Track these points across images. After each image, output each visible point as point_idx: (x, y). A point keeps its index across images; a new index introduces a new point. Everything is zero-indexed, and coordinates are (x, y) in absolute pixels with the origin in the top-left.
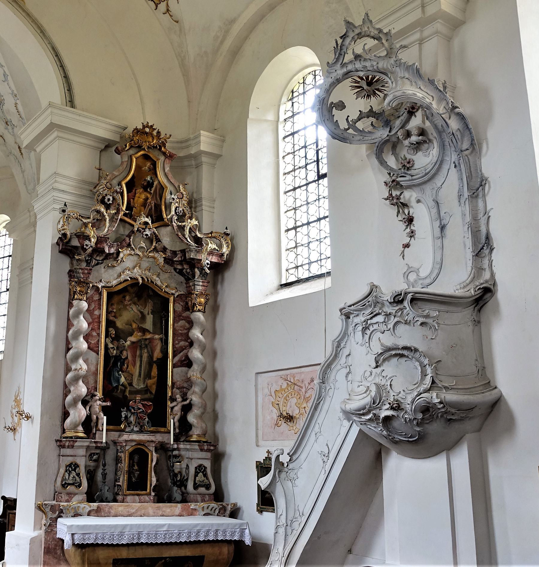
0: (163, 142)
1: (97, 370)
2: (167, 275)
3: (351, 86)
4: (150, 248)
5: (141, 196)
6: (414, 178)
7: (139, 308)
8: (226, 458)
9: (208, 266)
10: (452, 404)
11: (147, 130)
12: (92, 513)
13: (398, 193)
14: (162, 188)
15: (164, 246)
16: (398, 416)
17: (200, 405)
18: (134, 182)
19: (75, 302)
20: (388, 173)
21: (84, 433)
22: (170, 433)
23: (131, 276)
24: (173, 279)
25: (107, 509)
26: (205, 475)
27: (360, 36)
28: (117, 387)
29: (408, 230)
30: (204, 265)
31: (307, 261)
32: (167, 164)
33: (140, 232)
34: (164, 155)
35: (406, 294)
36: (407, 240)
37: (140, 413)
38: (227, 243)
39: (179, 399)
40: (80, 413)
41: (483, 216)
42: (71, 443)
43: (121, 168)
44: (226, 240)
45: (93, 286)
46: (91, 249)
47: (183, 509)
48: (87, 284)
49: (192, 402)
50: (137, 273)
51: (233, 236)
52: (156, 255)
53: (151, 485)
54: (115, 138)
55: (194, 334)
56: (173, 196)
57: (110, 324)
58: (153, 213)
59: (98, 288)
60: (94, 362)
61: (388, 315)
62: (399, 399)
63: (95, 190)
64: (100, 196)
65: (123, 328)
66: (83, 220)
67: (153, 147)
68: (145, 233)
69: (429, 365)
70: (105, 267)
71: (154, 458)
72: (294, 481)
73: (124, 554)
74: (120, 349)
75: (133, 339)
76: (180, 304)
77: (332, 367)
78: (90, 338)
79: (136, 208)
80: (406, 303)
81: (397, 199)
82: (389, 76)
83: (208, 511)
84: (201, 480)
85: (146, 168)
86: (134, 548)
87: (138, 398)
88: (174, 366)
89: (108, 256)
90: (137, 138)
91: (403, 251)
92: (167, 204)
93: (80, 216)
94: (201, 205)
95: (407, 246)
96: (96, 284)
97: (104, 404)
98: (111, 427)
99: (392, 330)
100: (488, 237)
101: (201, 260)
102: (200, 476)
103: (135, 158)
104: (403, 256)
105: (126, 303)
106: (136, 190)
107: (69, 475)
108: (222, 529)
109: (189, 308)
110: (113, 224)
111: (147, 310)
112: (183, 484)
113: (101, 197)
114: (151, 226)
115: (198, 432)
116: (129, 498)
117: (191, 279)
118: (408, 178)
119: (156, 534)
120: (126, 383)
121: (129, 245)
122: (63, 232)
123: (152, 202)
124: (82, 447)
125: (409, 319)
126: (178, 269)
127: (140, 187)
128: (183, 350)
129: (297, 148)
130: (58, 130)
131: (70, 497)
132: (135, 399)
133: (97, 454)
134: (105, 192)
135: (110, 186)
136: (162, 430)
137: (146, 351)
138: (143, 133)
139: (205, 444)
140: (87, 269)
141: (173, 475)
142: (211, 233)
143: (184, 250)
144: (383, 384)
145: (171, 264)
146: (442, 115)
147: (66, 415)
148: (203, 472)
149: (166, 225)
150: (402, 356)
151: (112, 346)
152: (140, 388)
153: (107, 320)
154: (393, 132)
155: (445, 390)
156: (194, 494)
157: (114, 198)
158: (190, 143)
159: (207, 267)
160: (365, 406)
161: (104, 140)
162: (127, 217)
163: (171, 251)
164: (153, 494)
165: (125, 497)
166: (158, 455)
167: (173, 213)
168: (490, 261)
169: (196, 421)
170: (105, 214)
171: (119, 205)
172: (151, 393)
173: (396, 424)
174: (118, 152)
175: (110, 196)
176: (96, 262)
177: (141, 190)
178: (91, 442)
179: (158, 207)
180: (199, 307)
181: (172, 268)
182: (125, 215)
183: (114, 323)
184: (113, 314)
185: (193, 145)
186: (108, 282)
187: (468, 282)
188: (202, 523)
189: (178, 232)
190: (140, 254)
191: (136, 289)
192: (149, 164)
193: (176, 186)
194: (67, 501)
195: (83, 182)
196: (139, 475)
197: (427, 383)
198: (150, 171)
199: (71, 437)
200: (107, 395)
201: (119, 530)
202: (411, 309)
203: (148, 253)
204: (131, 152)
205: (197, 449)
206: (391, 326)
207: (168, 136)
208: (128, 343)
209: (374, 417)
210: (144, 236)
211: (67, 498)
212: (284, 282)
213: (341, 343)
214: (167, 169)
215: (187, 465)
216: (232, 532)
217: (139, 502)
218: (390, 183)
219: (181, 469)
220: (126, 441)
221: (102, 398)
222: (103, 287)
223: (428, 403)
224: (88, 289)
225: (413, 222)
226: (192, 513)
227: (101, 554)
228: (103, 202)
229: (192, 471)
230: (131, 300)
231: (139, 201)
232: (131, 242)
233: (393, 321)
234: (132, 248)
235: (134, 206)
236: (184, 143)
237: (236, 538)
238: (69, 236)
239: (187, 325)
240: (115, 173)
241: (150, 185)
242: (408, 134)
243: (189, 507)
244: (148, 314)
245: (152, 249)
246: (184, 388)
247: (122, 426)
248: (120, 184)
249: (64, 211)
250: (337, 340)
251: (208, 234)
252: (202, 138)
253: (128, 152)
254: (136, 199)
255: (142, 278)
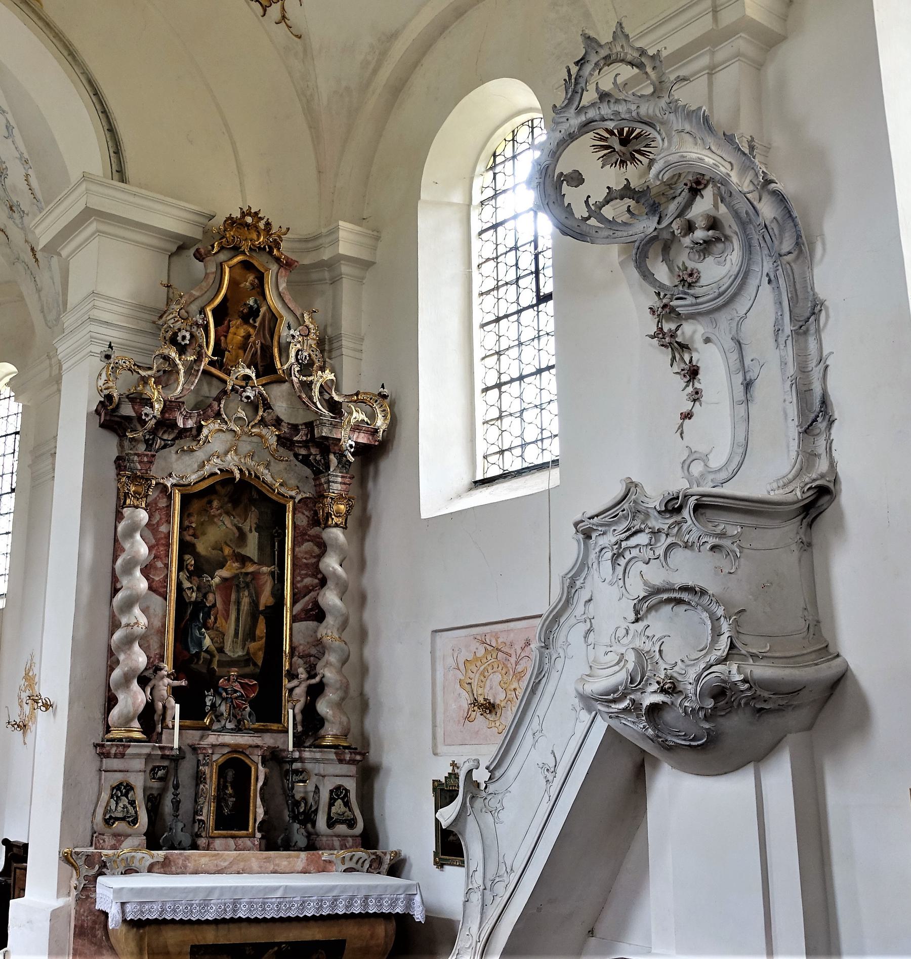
0: (276, 240)
1: (164, 625)
2: (282, 465)
3: (593, 146)
4: (253, 420)
5: (238, 331)
6: (699, 300)
7: (235, 521)
8: (382, 774)
9: (352, 450)
10: (764, 684)
11: (249, 220)
12: (156, 868)
13: (673, 326)
14: (274, 318)
15: (278, 417)
16: (672, 703)
17: (338, 685)
18: (226, 308)
19: (127, 512)
20: (655, 292)
21: (142, 732)
22: (287, 732)
23: (221, 467)
24: (293, 472)
25: (181, 862)
26: (347, 804)
27: (609, 60)
28: (198, 655)
29: (690, 389)
30: (345, 449)
31: (518, 442)
32: (281, 277)
33: (237, 392)
34: (277, 262)
35: (686, 497)
36: (687, 406)
37: (236, 698)
38: (384, 410)
39: (303, 675)
40: (135, 698)
41: (816, 366)
42: (121, 749)
43: (204, 284)
44: (382, 406)
45: (157, 484)
46: (153, 421)
47: (309, 861)
48: (147, 480)
49: (324, 680)
50: (231, 462)
51: (394, 399)
52: (264, 431)
53: (255, 820)
54: (195, 233)
55: (328, 566)
56: (292, 332)
57: (186, 547)
58: (259, 360)
59: (165, 486)
60: (159, 612)
61: (656, 533)
62: (675, 675)
63: (160, 322)
64: (170, 331)
65: (208, 554)
66: (140, 372)
67: (259, 248)
68: (244, 394)
69: (725, 618)
70: (177, 452)
71: (260, 774)
72: (496, 814)
73: (210, 937)
74: (202, 590)
75: (224, 573)
76: (303, 514)
77: (562, 620)
78: (153, 572)
79: (229, 351)
80: (686, 513)
81: (672, 336)
82: (658, 129)
83: (352, 864)
84: (339, 812)
85: (247, 284)
86: (226, 926)
87: (234, 672)
88: (294, 619)
89: (183, 433)
90: (232, 233)
91: (682, 425)
92: (283, 346)
93: (135, 365)
94: (340, 347)
95: (688, 416)
96: (162, 481)
97: (176, 683)
98: (188, 723)
99: (662, 558)
100: (825, 402)
101: (340, 440)
102: (339, 805)
103: (228, 267)
104: (682, 434)
105: (213, 512)
106: (230, 321)
107: (117, 804)
108: (375, 894)
109: (320, 521)
110: (192, 378)
111: (249, 524)
112: (308, 818)
113: (170, 333)
114: (255, 381)
115: (335, 732)
116: (218, 842)
117: (323, 473)
118: (690, 300)
119: (264, 903)
120: (213, 648)
121: (218, 415)
122: (106, 392)
123: (256, 342)
124: (138, 755)
125: (691, 540)
126: (300, 455)
127: (237, 317)
128: (310, 592)
129: (501, 250)
130: (98, 220)
131: (118, 841)
132: (228, 674)
133: (164, 767)
134: (178, 325)
135: (186, 314)
136: (275, 726)
137: (246, 593)
138: (241, 224)
139: (347, 751)
140: (147, 455)
141: (292, 803)
142: (357, 394)
143: (312, 423)
144: (647, 649)
145: (289, 447)
146: (748, 195)
147: (111, 701)
148: (342, 799)
149: (281, 381)
150: (679, 602)
151: (189, 585)
152: (236, 655)
153: (182, 542)
154: (664, 224)
155: (753, 659)
156: (327, 836)
157: (192, 335)
158: (320, 241)
159: (350, 452)
160: (617, 687)
161: (176, 236)
162: (214, 367)
163: (289, 424)
164: (258, 835)
165: (211, 840)
166: (267, 770)
167: (292, 360)
168: (829, 441)
169: (330, 712)
170: (178, 361)
171: (201, 346)
172: (255, 664)
173: (669, 717)
174: (199, 256)
175: (187, 331)
176: (163, 443)
177: (239, 321)
178: (154, 748)
179: (267, 351)
180: (336, 520)
181: (291, 453)
182: (211, 363)
183: (193, 546)
184: (191, 531)
185: (326, 246)
186: (182, 478)
187: (790, 476)
188: (342, 885)
189: (300, 392)
190: (237, 429)
191: (229, 488)
192: (251, 278)
193: (298, 314)
194: (114, 847)
195: (140, 308)
196: (235, 803)
197: (722, 647)
198: (253, 289)
199: (121, 740)
200: (181, 667)
201: (201, 896)
202: (695, 522)
203: (250, 428)
204: (222, 257)
205: (332, 760)
206: (660, 551)
207: (284, 230)
208: (217, 580)
209: (632, 706)
210: (243, 399)
211: (113, 842)
212: (479, 477)
213: (577, 580)
214: (283, 286)
215: (317, 787)
216: (392, 899)
217: (235, 850)
218: (660, 309)
219: (306, 792)
220: (213, 746)
221: (172, 674)
222: (174, 485)
223: (724, 681)
224: (148, 490)
225: (698, 376)
226: (324, 867)
227: (172, 937)
228: (173, 341)
229: (325, 796)
230: (221, 507)
231: (235, 341)
232: (222, 409)
233: (664, 542)
234: (224, 419)
235: (226, 349)
236: (312, 241)
237: (399, 910)
238: (116, 399)
239: (317, 550)
240: (194, 292)
241: (253, 313)
242: (690, 227)
243: (320, 857)
244: (251, 531)
245: (256, 421)
246: (311, 656)
247: (207, 721)
248: (202, 311)
249: (108, 357)
250: (570, 575)
251: (352, 395)
252: (342, 234)
253: (216, 257)
254: (230, 336)
255: (241, 470)
